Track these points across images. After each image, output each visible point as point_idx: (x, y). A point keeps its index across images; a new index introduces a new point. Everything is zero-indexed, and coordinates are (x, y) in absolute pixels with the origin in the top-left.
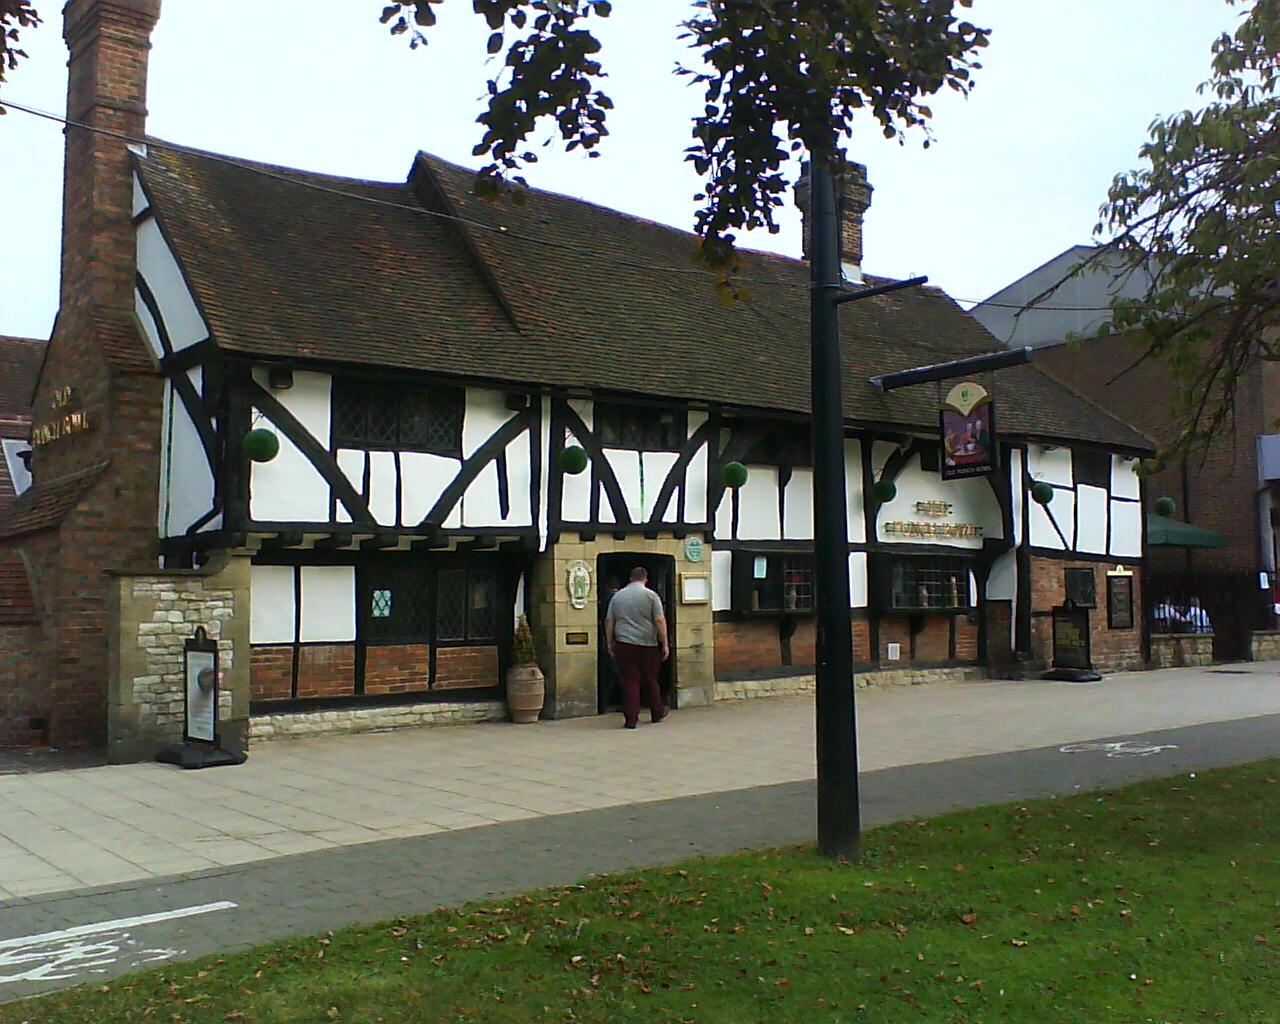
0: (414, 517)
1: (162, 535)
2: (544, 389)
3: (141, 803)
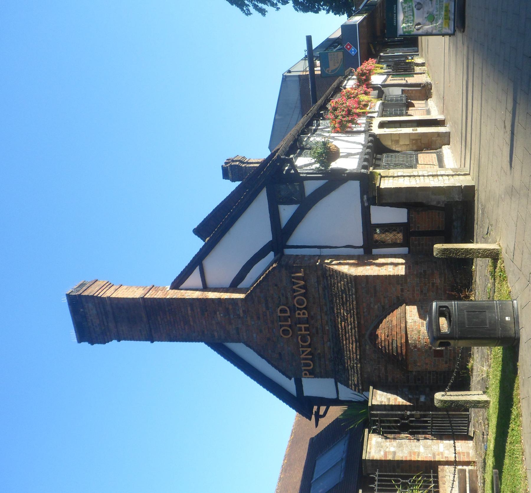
1: (361, 251)
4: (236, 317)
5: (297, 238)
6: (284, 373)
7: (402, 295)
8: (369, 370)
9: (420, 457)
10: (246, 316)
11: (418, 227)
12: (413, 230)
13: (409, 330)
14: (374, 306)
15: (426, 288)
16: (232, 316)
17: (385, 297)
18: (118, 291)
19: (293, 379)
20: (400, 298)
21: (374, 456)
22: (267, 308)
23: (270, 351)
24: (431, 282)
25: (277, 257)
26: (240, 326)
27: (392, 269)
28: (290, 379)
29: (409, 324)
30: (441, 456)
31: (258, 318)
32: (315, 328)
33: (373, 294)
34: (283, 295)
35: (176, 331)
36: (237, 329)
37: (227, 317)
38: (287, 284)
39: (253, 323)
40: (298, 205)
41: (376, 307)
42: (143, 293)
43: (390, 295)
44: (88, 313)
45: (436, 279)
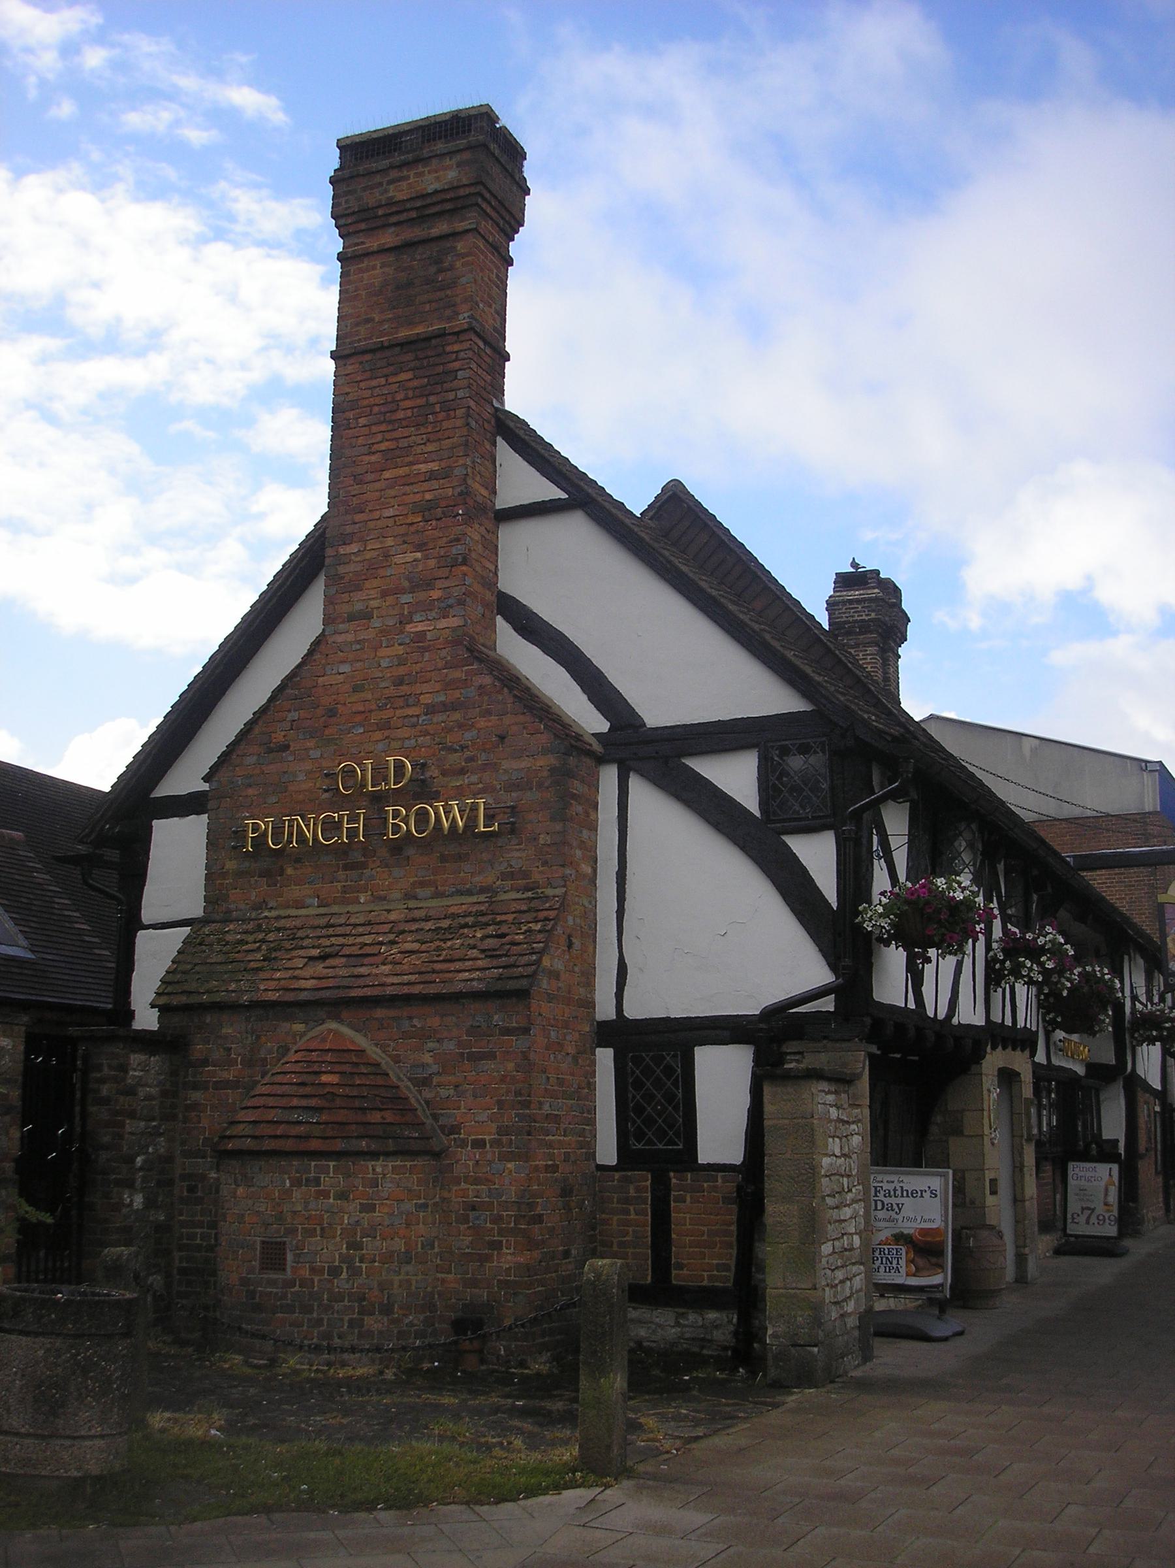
1: (605, 1010)
7: (463, 1144)
8: (227, 1030)
12: (674, 1181)
16: (406, 598)
18: (493, 255)
19: (206, 787)
22: (431, 710)
23: (294, 715)
25: (593, 741)
26: (376, 623)
28: (206, 779)
29: (370, 1164)
31: (399, 682)
36: (367, 615)
37: (406, 584)
39: (384, 664)
40: (757, 814)
41: (427, 1058)
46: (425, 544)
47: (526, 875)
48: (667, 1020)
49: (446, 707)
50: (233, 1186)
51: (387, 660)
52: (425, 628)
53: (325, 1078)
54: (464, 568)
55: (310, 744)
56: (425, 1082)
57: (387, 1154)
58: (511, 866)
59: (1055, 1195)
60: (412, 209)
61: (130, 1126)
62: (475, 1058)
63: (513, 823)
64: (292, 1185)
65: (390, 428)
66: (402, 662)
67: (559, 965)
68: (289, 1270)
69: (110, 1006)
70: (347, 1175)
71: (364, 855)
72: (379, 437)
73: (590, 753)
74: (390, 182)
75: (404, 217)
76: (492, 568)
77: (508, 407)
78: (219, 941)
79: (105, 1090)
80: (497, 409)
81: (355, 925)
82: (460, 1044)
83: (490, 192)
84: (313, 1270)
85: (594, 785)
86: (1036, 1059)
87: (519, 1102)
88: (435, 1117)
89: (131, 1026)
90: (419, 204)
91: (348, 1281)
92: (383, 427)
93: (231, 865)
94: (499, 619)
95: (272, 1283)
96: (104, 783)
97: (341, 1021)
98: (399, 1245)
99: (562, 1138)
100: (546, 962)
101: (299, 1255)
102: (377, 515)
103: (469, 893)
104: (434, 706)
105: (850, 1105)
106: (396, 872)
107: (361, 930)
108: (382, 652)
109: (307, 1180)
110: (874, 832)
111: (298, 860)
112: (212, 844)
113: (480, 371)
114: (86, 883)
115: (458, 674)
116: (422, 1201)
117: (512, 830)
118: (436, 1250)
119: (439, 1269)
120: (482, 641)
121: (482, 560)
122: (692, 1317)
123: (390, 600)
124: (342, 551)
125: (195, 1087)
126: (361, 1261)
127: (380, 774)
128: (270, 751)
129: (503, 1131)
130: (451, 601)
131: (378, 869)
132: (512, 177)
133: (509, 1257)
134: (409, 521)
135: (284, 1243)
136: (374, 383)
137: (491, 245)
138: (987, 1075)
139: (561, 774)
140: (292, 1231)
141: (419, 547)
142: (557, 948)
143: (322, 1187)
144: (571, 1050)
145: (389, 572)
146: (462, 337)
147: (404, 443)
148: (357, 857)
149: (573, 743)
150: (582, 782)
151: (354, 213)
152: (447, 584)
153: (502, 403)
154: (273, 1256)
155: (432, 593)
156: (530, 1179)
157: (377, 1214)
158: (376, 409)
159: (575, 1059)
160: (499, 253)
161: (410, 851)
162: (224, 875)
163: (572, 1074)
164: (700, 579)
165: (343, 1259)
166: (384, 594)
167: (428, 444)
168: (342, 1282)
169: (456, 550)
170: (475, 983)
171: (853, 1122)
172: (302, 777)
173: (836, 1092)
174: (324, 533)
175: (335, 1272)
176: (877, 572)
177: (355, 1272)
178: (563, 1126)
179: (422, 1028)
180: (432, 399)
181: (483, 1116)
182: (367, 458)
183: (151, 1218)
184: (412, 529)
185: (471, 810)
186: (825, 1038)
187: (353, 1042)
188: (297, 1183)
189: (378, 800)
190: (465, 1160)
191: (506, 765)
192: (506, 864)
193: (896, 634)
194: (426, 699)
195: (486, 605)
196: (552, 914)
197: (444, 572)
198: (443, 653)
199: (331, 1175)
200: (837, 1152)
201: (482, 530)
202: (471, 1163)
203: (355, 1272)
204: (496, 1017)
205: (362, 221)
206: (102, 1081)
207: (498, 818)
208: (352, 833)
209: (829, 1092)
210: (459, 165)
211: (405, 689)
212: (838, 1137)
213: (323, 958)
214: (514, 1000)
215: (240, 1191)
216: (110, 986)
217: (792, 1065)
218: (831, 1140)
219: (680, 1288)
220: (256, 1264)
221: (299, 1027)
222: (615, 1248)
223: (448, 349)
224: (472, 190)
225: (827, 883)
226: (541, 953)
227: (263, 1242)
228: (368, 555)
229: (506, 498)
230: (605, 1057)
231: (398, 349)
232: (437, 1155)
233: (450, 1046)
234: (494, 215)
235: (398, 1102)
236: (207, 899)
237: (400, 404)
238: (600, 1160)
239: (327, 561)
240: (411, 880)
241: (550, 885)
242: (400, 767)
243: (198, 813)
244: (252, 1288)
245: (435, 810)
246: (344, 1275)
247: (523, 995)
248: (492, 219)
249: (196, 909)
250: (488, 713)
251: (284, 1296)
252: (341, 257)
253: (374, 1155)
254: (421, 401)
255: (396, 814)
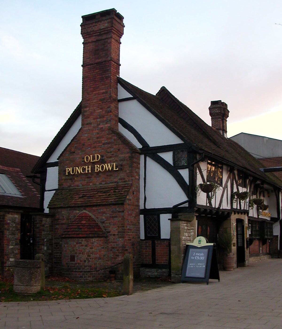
0: (217, 207)
1: (142, 207)
2: (215, 170)
3: (82, 309)
4: (99, 123)
5: (151, 164)
6: (61, 155)
7: (111, 235)
8: (63, 213)
9: (6, 246)
10: (99, 129)
11: (157, 246)
12: (156, 242)
13: (192, 258)
14: (104, 216)
15: (116, 251)
16: (99, 120)
17: (110, 223)
18: (116, 42)
19: (58, 161)
20: (109, 233)
21: (7, 216)
22: (104, 144)
23: (76, 145)
24: (119, 254)
25: (138, 150)
26: (92, 125)
27: (129, 228)
28: (58, 159)
29: (92, 239)
30: (7, 259)
31: (98, 138)
32: (91, 176)
33: (111, 216)
34: (113, 154)
35: (89, 82)
36: (90, 124)
37: (98, 117)
38: (120, 157)
39: (94, 134)
40: (173, 165)
41: (104, 218)
42: (114, 59)
43: (111, 227)
44: (101, 23)
45: (121, 257)
46: (102, 108)
47: (124, 179)
48: (154, 209)
49: (107, 143)
50: (64, 245)
51: (95, 133)
52: (103, 126)
53: (83, 222)
54: (111, 113)
55: (79, 151)
56: (103, 222)
57: (95, 237)
58: (121, 177)
59: (259, 248)
60: (98, 33)
61: (43, 233)
62: (113, 217)
63: (121, 168)
64: (76, 244)
65: (94, 82)
66: (98, 134)
67: (131, 198)
68: (76, 261)
69: (39, 207)
70: (87, 242)
71: (91, 175)
72: (92, 84)
73: (138, 153)
74: (93, 26)
75: (97, 34)
76: (117, 112)
77: (120, 77)
78: (61, 194)
79: (38, 226)
80: (118, 77)
81: (89, 190)
82: (110, 215)
83: (115, 28)
84: (81, 261)
85: (139, 159)
86: (249, 215)
87: (122, 226)
88: (105, 230)
89: (44, 212)
90: (100, 31)
91: (87, 263)
92: (93, 82)
93: (64, 178)
94: (119, 123)
95: (72, 264)
96: (40, 155)
97: (86, 210)
98: (98, 256)
99: (132, 234)
100: (128, 197)
101: (78, 258)
102: (92, 101)
103: (113, 183)
104: (105, 143)
105: (190, 226)
106: (98, 179)
107: (90, 191)
108: (94, 131)
109: (79, 243)
110: (197, 169)
111: (77, 176)
112: (59, 173)
113: (114, 69)
114: (33, 182)
115: (110, 136)
116: (103, 247)
117: (121, 170)
118: (106, 257)
119: (107, 261)
120: (115, 129)
121: (115, 111)
122: (160, 270)
123: (95, 120)
124: (85, 109)
125: (57, 224)
126: (90, 259)
127: (94, 158)
128: (71, 153)
129: (119, 232)
130: (108, 120)
131: (94, 178)
132: (120, 24)
133: (120, 258)
134: (99, 103)
135: (75, 256)
136: (91, 72)
137: (116, 40)
138: (232, 220)
139: (131, 158)
140: (76, 253)
141: (101, 109)
142: (130, 194)
143: (82, 244)
144: (134, 215)
145: (95, 114)
146: (109, 62)
147: (97, 86)
148: (89, 175)
149: (134, 150)
150: (136, 159)
151: (86, 33)
152: (107, 117)
153: (119, 76)
154: (73, 258)
155: (104, 119)
156: (124, 242)
157: (93, 249)
158: (91, 78)
159: (135, 217)
160: (118, 42)
161: (100, 174)
162: (62, 180)
163: (134, 220)
164: (160, 115)
165: (87, 259)
166: (94, 119)
167: (103, 86)
168: (86, 264)
169: (109, 109)
170: (113, 202)
171: (191, 230)
172: (78, 159)
173: (186, 223)
174: (81, 105)
175: (85, 261)
176: (221, 101)
177: (89, 261)
178: (132, 231)
179: (103, 211)
180: (103, 76)
181: (115, 229)
182: (90, 89)
183: (48, 252)
184: (100, 105)
185: (112, 165)
186: (186, 212)
187: (88, 214)
188: (77, 243)
189: (94, 163)
190: (111, 238)
191: (120, 156)
192: (120, 177)
193: (226, 116)
194: (103, 142)
195: (116, 121)
196: (129, 187)
197: (106, 114)
198: (106, 132)
199: (84, 241)
200: (187, 235)
201: (115, 104)
202: (113, 239)
203: (89, 261)
204: (117, 209)
205: (87, 35)
206: (37, 224)
207: (118, 167)
208: (88, 171)
209: (185, 223)
210: (108, 23)
211: (99, 140)
212: (187, 233)
213: (83, 197)
214: (121, 205)
215: (66, 245)
216: (39, 204)
217: (180, 218)
218: (185, 233)
219: (157, 264)
220: (69, 260)
221: (78, 212)
222: (144, 257)
223: (106, 65)
224: (111, 28)
225: (187, 179)
226: (126, 196)
227: (70, 256)
228: (90, 111)
229: (120, 97)
230: (142, 217)
231: (96, 65)
232: (106, 237)
233: (108, 215)
234: (116, 33)
235: (97, 226)
236: (59, 185)
237: (97, 77)
238: (141, 238)
239: (82, 112)
240: (101, 180)
241: (129, 181)
242: (98, 157)
243: (57, 166)
244: (68, 265)
245: (105, 166)
246: (87, 262)
247: (122, 204)
248: (115, 34)
249: (56, 187)
250: (116, 145)
251: (75, 266)
252: (83, 43)
253: (92, 237)
254: (101, 76)
255: (97, 167)
